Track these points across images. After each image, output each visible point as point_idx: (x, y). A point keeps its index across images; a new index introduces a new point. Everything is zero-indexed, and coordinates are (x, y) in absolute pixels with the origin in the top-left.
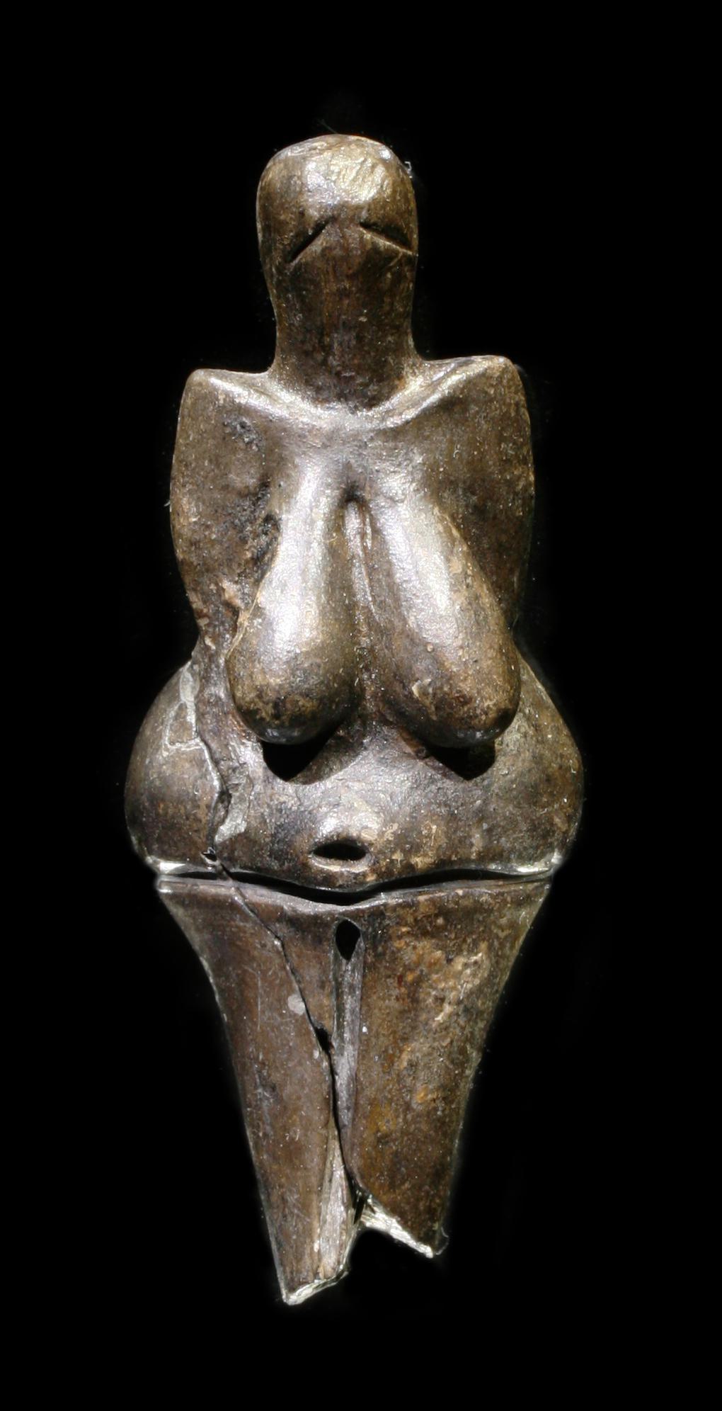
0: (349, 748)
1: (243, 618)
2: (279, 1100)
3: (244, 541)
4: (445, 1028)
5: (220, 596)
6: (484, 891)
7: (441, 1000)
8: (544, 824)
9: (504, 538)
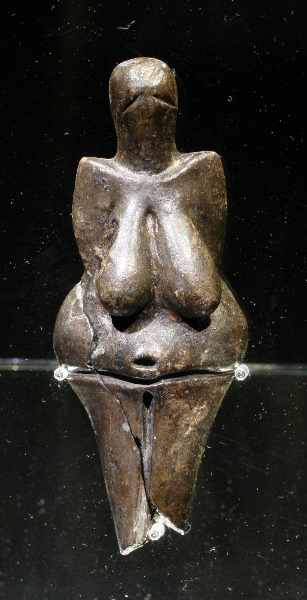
0: (148, 318)
1: (104, 263)
2: (118, 468)
3: (104, 230)
4: (189, 437)
5: (94, 253)
6: (206, 379)
7: (187, 425)
8: (231, 350)
9: (214, 229)
